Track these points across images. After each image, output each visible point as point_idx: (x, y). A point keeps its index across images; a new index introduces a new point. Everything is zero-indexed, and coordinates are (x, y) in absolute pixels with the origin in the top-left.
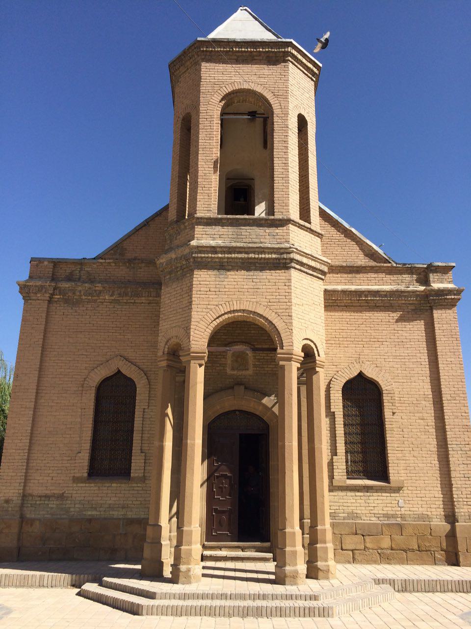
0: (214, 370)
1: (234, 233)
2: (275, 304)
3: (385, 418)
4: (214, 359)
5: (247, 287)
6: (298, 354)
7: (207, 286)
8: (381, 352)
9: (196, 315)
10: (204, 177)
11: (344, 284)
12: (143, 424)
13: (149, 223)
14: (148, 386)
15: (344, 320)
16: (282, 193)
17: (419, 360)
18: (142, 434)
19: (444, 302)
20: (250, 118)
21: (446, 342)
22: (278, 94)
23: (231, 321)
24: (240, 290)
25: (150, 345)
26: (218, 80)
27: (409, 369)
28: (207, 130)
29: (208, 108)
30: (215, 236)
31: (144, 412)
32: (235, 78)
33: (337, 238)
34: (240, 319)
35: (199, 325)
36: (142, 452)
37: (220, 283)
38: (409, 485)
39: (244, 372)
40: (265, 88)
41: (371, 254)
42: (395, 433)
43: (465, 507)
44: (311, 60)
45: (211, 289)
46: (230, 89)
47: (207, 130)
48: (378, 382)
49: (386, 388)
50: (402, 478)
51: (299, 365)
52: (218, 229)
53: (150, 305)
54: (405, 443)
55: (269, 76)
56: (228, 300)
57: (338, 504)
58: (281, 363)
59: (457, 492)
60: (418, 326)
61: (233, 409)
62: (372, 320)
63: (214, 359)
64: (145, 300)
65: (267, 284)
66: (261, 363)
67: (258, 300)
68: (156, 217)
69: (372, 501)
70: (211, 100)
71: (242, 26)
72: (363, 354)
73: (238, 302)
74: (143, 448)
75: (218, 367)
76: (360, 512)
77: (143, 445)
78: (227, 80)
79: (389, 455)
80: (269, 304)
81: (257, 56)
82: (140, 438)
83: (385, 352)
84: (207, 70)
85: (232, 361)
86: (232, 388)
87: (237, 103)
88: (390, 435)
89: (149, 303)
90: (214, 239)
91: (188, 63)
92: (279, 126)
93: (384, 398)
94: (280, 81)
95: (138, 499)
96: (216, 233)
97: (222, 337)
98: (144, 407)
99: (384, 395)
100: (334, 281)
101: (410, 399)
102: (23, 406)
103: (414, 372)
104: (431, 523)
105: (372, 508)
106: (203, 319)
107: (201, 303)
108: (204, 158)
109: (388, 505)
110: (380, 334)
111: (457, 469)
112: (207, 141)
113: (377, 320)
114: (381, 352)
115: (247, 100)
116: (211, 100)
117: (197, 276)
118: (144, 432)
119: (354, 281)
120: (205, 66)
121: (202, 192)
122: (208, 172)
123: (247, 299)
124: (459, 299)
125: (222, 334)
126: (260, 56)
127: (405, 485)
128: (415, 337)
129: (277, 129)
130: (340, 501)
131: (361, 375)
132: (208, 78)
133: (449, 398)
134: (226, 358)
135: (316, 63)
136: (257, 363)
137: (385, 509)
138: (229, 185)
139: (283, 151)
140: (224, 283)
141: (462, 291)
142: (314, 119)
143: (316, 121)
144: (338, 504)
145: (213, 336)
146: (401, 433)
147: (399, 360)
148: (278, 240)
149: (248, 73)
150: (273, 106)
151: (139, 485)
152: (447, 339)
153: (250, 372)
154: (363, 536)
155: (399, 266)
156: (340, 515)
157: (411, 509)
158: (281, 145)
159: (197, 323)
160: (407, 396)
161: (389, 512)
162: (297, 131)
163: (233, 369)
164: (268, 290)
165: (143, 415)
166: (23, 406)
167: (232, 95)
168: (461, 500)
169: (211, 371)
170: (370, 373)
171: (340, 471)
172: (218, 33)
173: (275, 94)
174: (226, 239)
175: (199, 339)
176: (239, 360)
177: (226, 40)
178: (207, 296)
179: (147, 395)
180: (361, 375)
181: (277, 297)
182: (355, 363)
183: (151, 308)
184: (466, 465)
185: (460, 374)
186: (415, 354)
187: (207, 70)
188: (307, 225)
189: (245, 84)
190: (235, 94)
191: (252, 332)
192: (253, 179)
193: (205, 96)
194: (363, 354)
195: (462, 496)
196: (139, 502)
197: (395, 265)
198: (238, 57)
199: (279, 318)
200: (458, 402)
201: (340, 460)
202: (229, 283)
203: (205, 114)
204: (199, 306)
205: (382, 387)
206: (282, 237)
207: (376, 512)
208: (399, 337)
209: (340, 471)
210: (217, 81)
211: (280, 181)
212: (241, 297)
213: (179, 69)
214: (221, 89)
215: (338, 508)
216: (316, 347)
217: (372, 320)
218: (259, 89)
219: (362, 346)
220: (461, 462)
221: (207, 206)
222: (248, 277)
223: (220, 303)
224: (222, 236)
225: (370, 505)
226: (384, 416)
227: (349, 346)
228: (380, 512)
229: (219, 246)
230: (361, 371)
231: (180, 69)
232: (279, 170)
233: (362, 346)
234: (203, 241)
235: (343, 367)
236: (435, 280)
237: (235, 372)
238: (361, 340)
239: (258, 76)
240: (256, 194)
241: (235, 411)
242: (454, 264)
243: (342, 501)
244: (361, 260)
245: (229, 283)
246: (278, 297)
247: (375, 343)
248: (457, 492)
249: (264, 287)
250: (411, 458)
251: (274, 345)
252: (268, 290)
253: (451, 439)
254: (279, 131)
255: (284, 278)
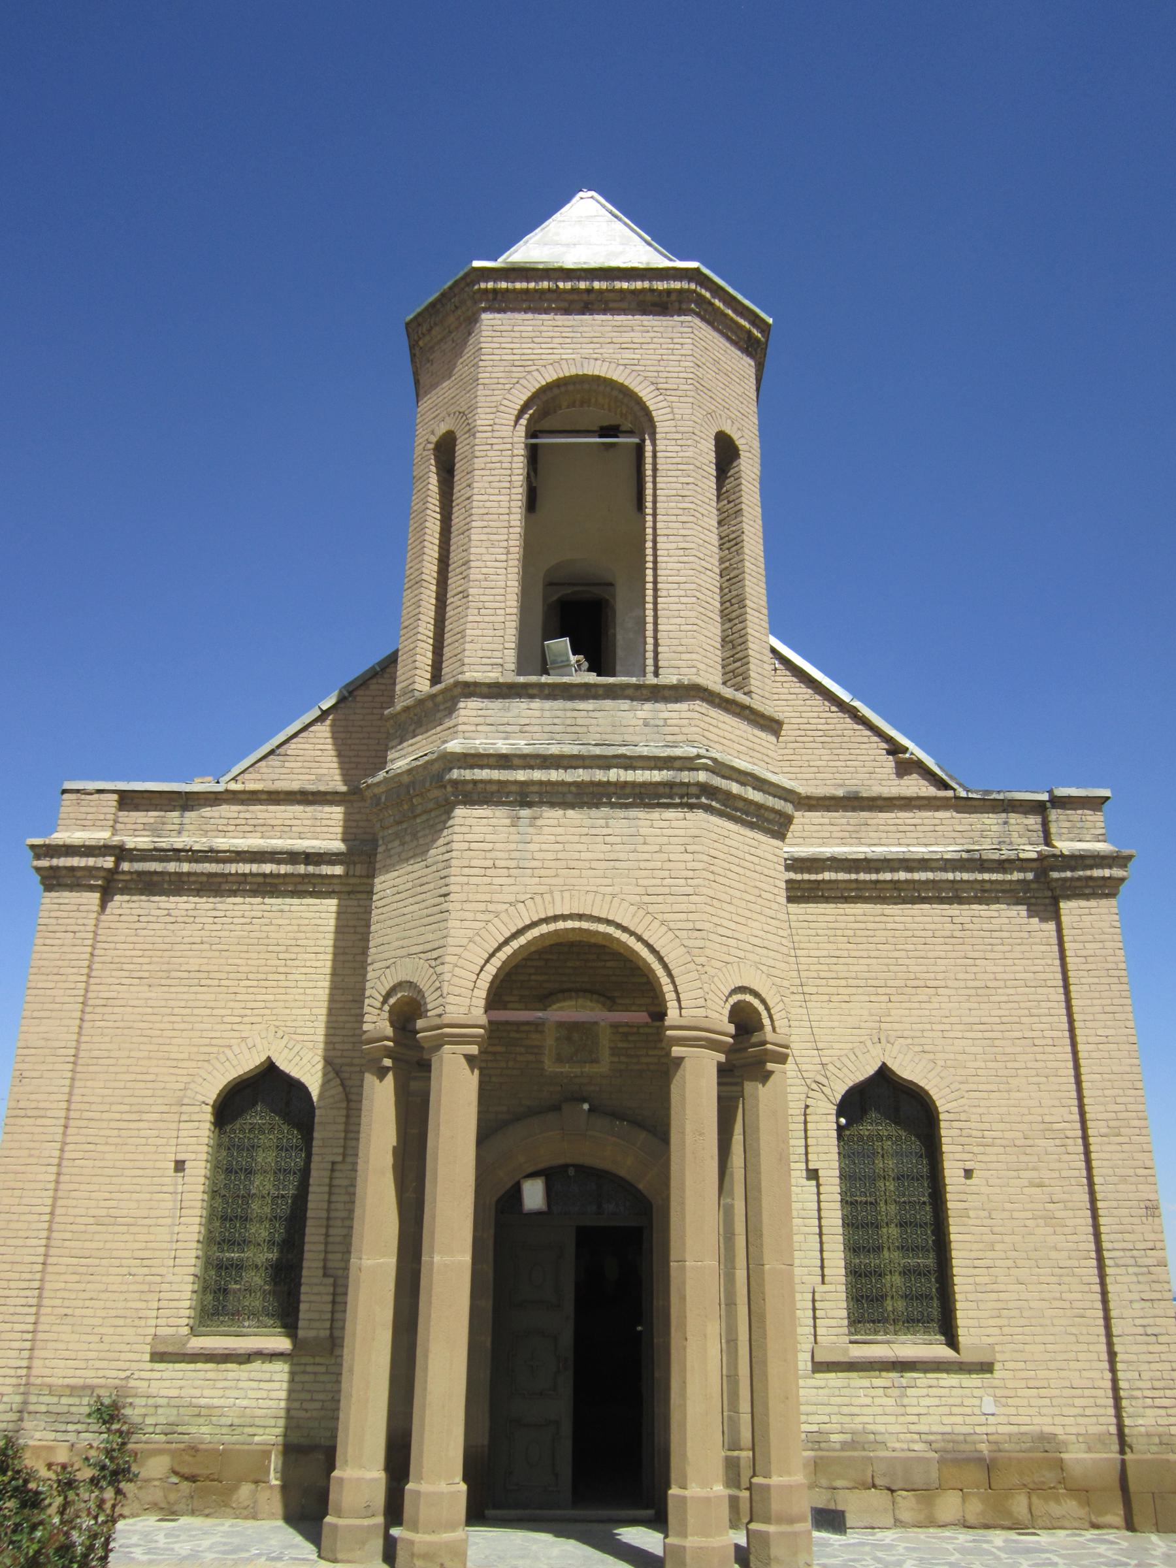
0: (511, 1064)
1: (556, 721)
2: (660, 899)
3: (945, 1185)
4: (513, 1035)
5: (589, 856)
6: (718, 1028)
7: (489, 855)
8: (934, 1012)
9: (458, 930)
10: (484, 584)
11: (839, 841)
12: (329, 1202)
13: (356, 693)
14: (344, 1105)
15: (839, 932)
16: (678, 621)
17: (1028, 1034)
18: (328, 1227)
19: (1087, 887)
20: (589, 443)
21: (1093, 987)
22: (665, 386)
23: (547, 943)
24: (572, 864)
25: (350, 998)
26: (517, 356)
27: (1005, 1058)
28: (493, 472)
29: (497, 421)
30: (509, 728)
31: (333, 1170)
32: (562, 351)
33: (820, 727)
34: (571, 937)
35: (466, 954)
36: (325, 1275)
37: (521, 846)
38: (1007, 1356)
39: (587, 1069)
40: (635, 374)
41: (907, 767)
42: (971, 1222)
43: (1149, 1412)
44: (747, 308)
45: (499, 863)
46: (551, 375)
47: (493, 472)
48: (927, 1093)
49: (948, 1107)
50: (990, 1340)
51: (722, 1058)
52: (522, 709)
53: (352, 896)
54: (998, 1247)
55: (644, 346)
56: (542, 889)
57: (828, 1409)
58: (676, 1051)
59: (1129, 1375)
60: (1023, 948)
61: (561, 1161)
62: (910, 933)
63: (513, 1035)
64: (341, 884)
65: (640, 848)
66: (632, 1045)
67: (617, 889)
68: (371, 678)
69: (914, 1401)
70: (505, 402)
71: (587, 233)
72: (888, 1019)
73: (567, 895)
74: (330, 1264)
75: (521, 1054)
76: (883, 1430)
77: (330, 1256)
78: (543, 357)
79: (956, 1280)
80: (646, 899)
81: (615, 301)
82: (322, 1239)
83: (942, 1012)
84: (494, 334)
85: (557, 1039)
86: (556, 1108)
87: (568, 407)
88: (961, 1229)
89: (349, 893)
90: (507, 736)
91: (451, 319)
92: (669, 460)
93: (943, 1132)
94: (671, 357)
95: (316, 1396)
96: (512, 721)
97: (533, 977)
98: (332, 1158)
99: (942, 1124)
100: (815, 835)
101: (1007, 1135)
102: (33, 1152)
103: (1016, 1065)
104: (1062, 1455)
105: (914, 1419)
106: (477, 938)
107: (471, 897)
108: (484, 537)
109: (955, 1410)
110: (932, 969)
111: (1127, 1313)
112: (492, 498)
113: (922, 933)
114: (934, 1012)
115: (593, 400)
116: (505, 402)
117: (464, 829)
118: (331, 1223)
119: (863, 835)
120: (488, 319)
121: (478, 619)
122: (492, 571)
123: (588, 888)
124: (1122, 880)
125: (532, 971)
126: (622, 300)
127: (998, 1357)
128: (1018, 976)
129: (665, 467)
130: (833, 1400)
131: (884, 1073)
132: (496, 351)
133: (1104, 1131)
134: (542, 1032)
135: (757, 316)
136: (620, 1045)
137: (946, 1420)
138: (555, 598)
139: (681, 519)
140: (531, 847)
141: (1129, 858)
142: (756, 444)
143: (761, 448)
144: (828, 1409)
145: (508, 974)
146: (988, 1222)
147: (980, 1035)
148: (669, 738)
149: (595, 340)
150: (654, 414)
151: (318, 1360)
152: (1096, 980)
153: (604, 1066)
154: (892, 1491)
155: (974, 796)
156: (834, 1437)
157: (1013, 1420)
158: (673, 505)
159: (459, 950)
160: (1001, 1126)
161: (958, 1429)
162: (714, 473)
163: (559, 1059)
164: (643, 865)
165: (331, 1178)
166: (33, 1152)
167: (556, 391)
168: (1138, 1393)
169: (503, 1064)
170: (908, 1070)
171: (833, 1322)
172: (531, 250)
173: (660, 386)
174: (537, 736)
175: (462, 998)
176: (576, 1036)
177: (541, 266)
178: (488, 880)
179: (342, 1127)
180: (884, 1073)
181: (666, 882)
182: (869, 1043)
183: (355, 903)
184: (1149, 1304)
185: (1128, 1069)
186: (1017, 1019)
187: (494, 334)
188: (740, 697)
189: (585, 365)
190: (563, 389)
191: (609, 964)
192: (611, 585)
193: (490, 392)
194: (888, 1019)
195: (1140, 1384)
196: (317, 1405)
197: (963, 794)
198: (571, 302)
199: (670, 935)
200: (1126, 1140)
201: (833, 1296)
202: (544, 847)
203: (489, 434)
204: (467, 906)
205: (938, 1103)
206: (676, 730)
207: (923, 1428)
208: (979, 976)
209: (833, 1322)
210: (517, 357)
211: (672, 593)
212: (573, 881)
213: (429, 331)
214: (529, 377)
215: (826, 1419)
216: (768, 1009)
217: (910, 933)
218: (618, 375)
219: (886, 998)
220: (1136, 1296)
221: (489, 654)
222: (593, 831)
223: (522, 897)
224: (527, 728)
225: (912, 1410)
226: (944, 1177)
227: (853, 998)
228: (935, 1429)
229: (518, 752)
230: (884, 1064)
231: (434, 332)
232: (670, 566)
233: (886, 998)
234: (478, 742)
235: (839, 1053)
236: (1064, 831)
237: (565, 1068)
238: (882, 983)
239: (618, 346)
240: (619, 620)
241: (567, 1166)
242: (1106, 793)
243: (839, 1400)
244: (888, 784)
245: (544, 847)
246: (667, 882)
247: (919, 991)
248: (1129, 1375)
249: (632, 856)
250: (1011, 1287)
251: (660, 1005)
252: (643, 865)
253: (1112, 1237)
254: (670, 473)
255: (682, 832)
